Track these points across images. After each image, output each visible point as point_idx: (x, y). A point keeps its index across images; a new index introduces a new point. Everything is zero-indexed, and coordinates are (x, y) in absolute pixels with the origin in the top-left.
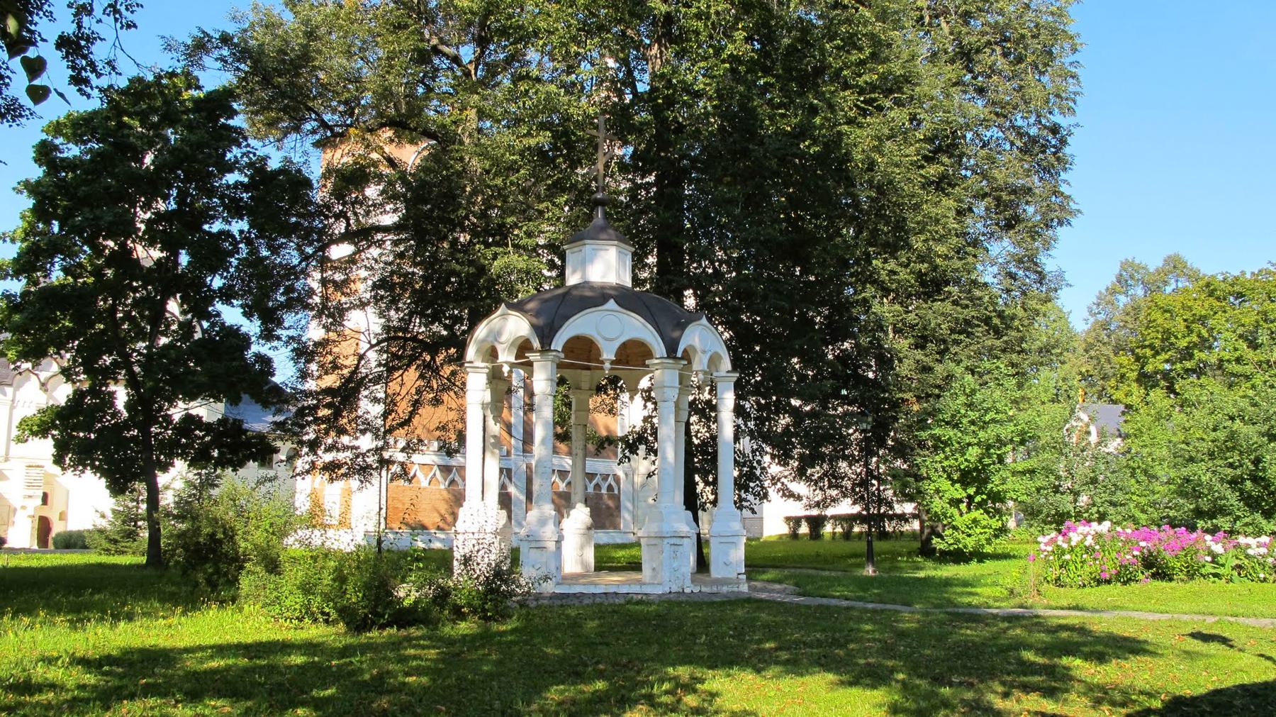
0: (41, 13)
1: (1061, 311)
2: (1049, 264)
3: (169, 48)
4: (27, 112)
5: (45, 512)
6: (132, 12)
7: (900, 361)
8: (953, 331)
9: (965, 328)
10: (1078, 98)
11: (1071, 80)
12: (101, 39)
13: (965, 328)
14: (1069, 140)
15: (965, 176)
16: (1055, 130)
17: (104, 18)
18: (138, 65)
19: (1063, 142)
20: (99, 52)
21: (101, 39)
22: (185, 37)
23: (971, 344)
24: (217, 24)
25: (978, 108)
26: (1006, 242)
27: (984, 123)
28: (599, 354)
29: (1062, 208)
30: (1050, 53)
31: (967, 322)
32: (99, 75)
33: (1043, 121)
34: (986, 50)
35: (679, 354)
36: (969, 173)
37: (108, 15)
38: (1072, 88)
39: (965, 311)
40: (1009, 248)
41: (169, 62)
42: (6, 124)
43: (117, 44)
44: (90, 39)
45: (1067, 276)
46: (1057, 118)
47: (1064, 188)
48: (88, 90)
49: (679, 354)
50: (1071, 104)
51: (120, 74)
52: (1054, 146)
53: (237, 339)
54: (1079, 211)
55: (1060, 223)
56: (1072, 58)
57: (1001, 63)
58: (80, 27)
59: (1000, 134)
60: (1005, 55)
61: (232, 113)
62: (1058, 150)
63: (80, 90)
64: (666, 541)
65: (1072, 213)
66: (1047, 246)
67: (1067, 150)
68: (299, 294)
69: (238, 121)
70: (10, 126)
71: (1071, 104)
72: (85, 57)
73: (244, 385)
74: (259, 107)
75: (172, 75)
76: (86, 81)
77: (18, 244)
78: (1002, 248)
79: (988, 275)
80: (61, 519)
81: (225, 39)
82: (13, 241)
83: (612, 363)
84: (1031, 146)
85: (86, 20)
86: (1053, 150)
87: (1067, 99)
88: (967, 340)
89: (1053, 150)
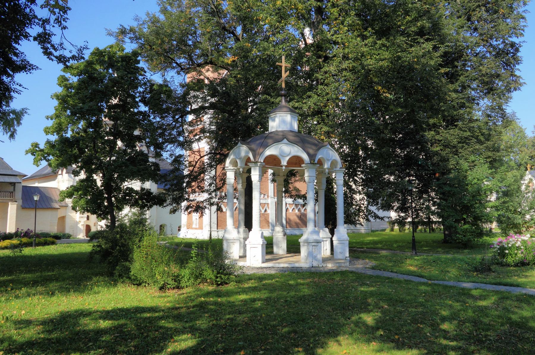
0: (35, 24)
1: (521, 128)
2: (509, 109)
3: (110, 34)
4: (35, 67)
5: (88, 223)
6: (66, 22)
7: (82, 297)
8: (459, 143)
9: (464, 141)
10: (525, 29)
11: (521, 20)
12: (55, 35)
13: (464, 141)
14: (520, 49)
15: (468, 70)
16: (513, 45)
17: (55, 25)
18: (73, 45)
19: (517, 50)
20: (55, 40)
21: (55, 35)
22: (115, 29)
23: (468, 148)
24: (129, 23)
25: (475, 38)
26: (486, 100)
27: (477, 44)
28: (281, 163)
29: (516, 81)
30: (511, 7)
31: (466, 138)
32: (56, 50)
33: (506, 41)
34: (477, 9)
35: (316, 162)
36: (469, 69)
37: (56, 24)
38: (522, 24)
39: (465, 133)
40: (487, 103)
41: (112, 41)
42: (25, 73)
43: (63, 36)
44: (49, 35)
45: (517, 115)
46: (514, 39)
47: (517, 73)
48: (53, 57)
49: (316, 162)
50: (522, 32)
51: (65, 49)
52: (512, 53)
53: (144, 157)
54: (525, 83)
55: (515, 89)
56: (523, 9)
57: (485, 15)
58: (45, 29)
59: (485, 49)
60: (487, 11)
61: (138, 62)
62: (514, 54)
63: (48, 58)
64: (310, 244)
65: (521, 85)
66: (507, 100)
67: (519, 54)
68: (175, 136)
69: (142, 65)
70: (27, 74)
71: (522, 32)
72: (49, 43)
73: (146, 175)
74: (149, 59)
75: (111, 47)
76: (51, 54)
77: (54, 120)
78: (485, 103)
79: (478, 114)
80: (94, 226)
81: (132, 30)
82: (52, 119)
83: (286, 166)
84: (499, 54)
85: (48, 27)
86: (512, 54)
87: (519, 29)
88: (466, 146)
89: (512, 54)
